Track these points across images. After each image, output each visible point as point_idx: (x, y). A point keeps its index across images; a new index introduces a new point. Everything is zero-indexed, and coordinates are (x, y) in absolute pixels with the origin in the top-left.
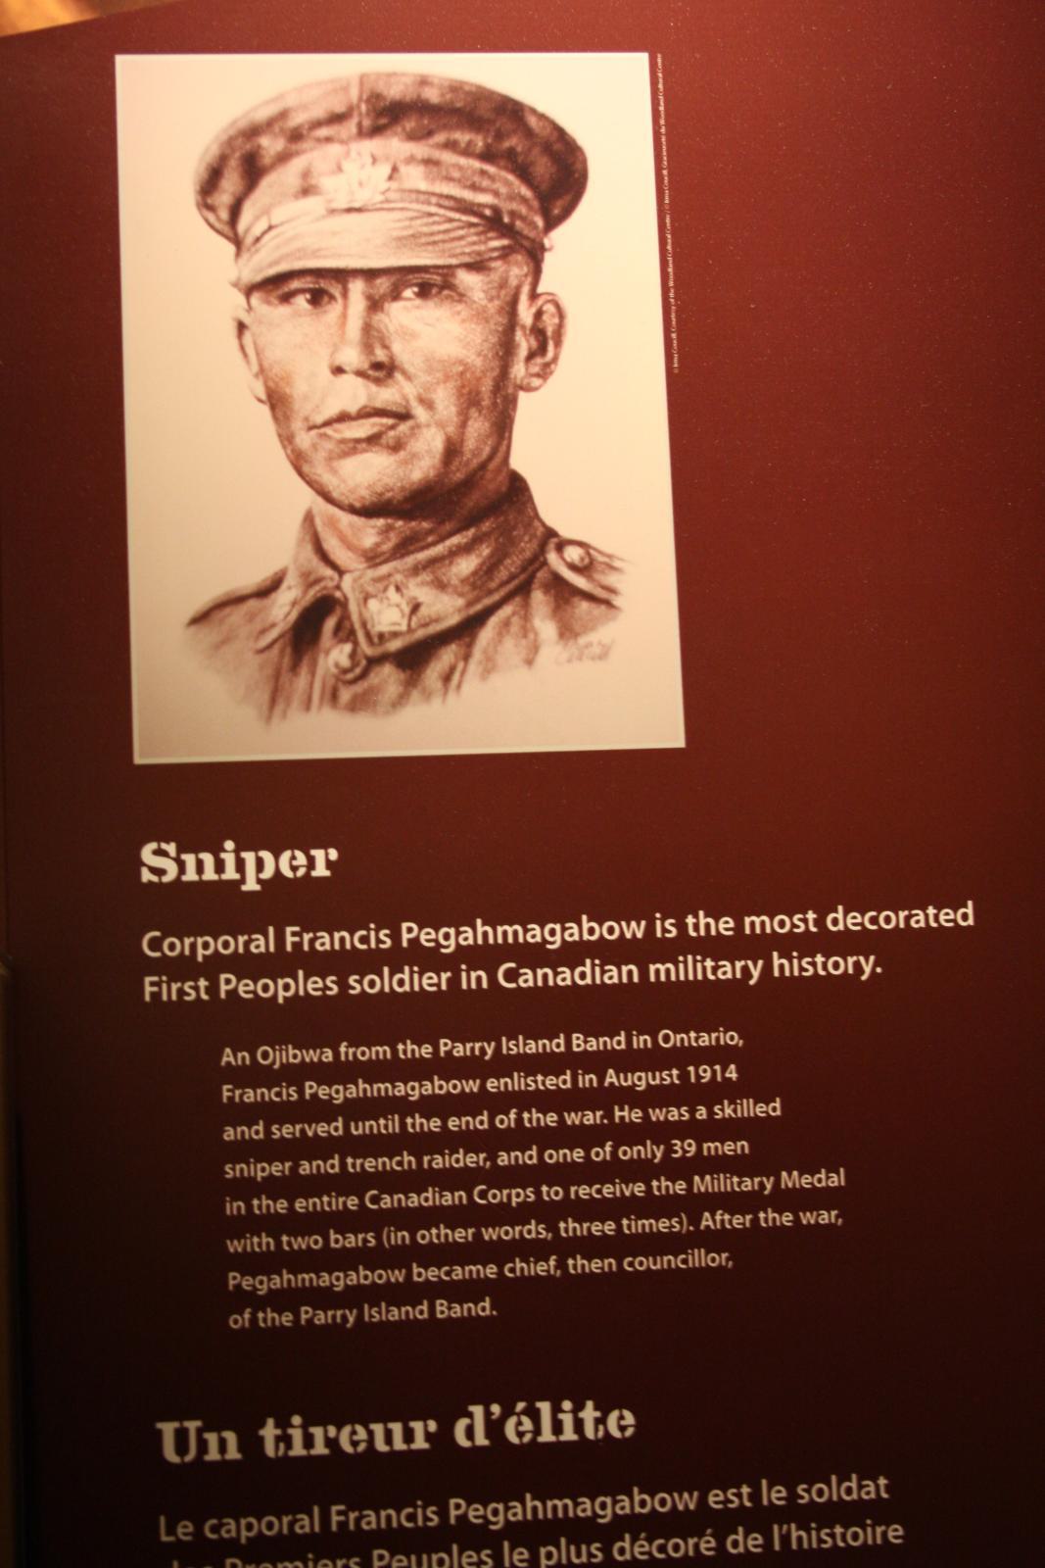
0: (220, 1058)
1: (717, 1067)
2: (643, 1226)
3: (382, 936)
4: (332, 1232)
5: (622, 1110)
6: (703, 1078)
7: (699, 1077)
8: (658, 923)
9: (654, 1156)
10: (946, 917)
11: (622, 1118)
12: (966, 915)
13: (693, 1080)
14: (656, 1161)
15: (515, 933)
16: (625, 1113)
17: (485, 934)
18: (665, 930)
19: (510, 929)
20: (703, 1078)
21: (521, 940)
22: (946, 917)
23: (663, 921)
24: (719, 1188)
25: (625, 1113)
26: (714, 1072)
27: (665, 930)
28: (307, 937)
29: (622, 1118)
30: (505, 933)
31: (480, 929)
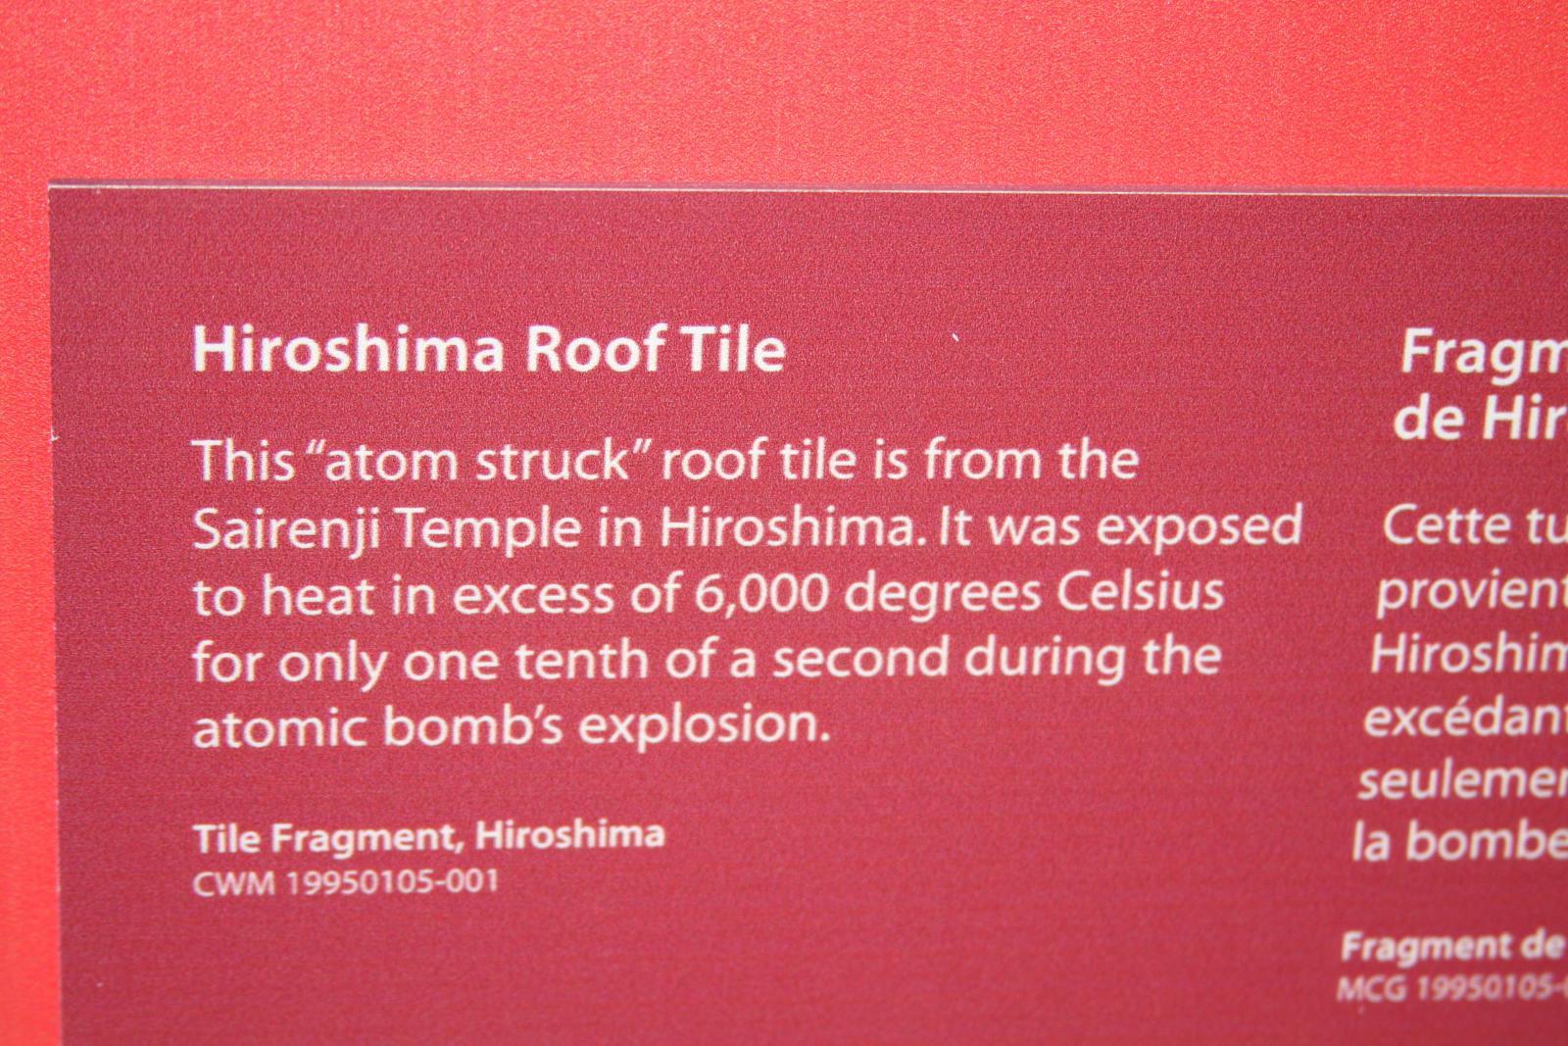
0: (201, 822)
1: (388, 874)
2: (368, 839)
3: (278, 458)
4: (1413, 825)
5: (214, 336)
6: (311, 888)
7: (302, 888)
8: (879, 454)
9: (363, 675)
10: (627, 834)
11: (490, 842)
12: (657, 837)
13: (295, 891)
14: (366, 688)
15: (452, 352)
16: (497, 834)
17: (373, 352)
18: (888, 467)
19: (441, 346)
20: (311, 888)
21: (462, 366)
22: (627, 834)
23: (887, 449)
24: (611, 538)
25: (497, 834)
26: (382, 880)
27: (888, 467)
28: (1443, 347)
29: (490, 842)
30: (431, 352)
31: (363, 343)
